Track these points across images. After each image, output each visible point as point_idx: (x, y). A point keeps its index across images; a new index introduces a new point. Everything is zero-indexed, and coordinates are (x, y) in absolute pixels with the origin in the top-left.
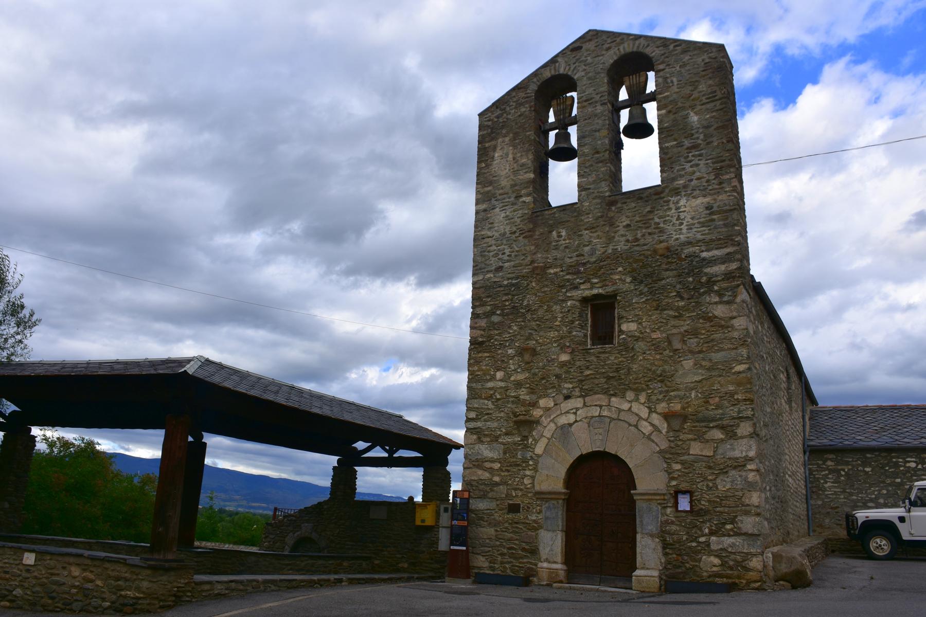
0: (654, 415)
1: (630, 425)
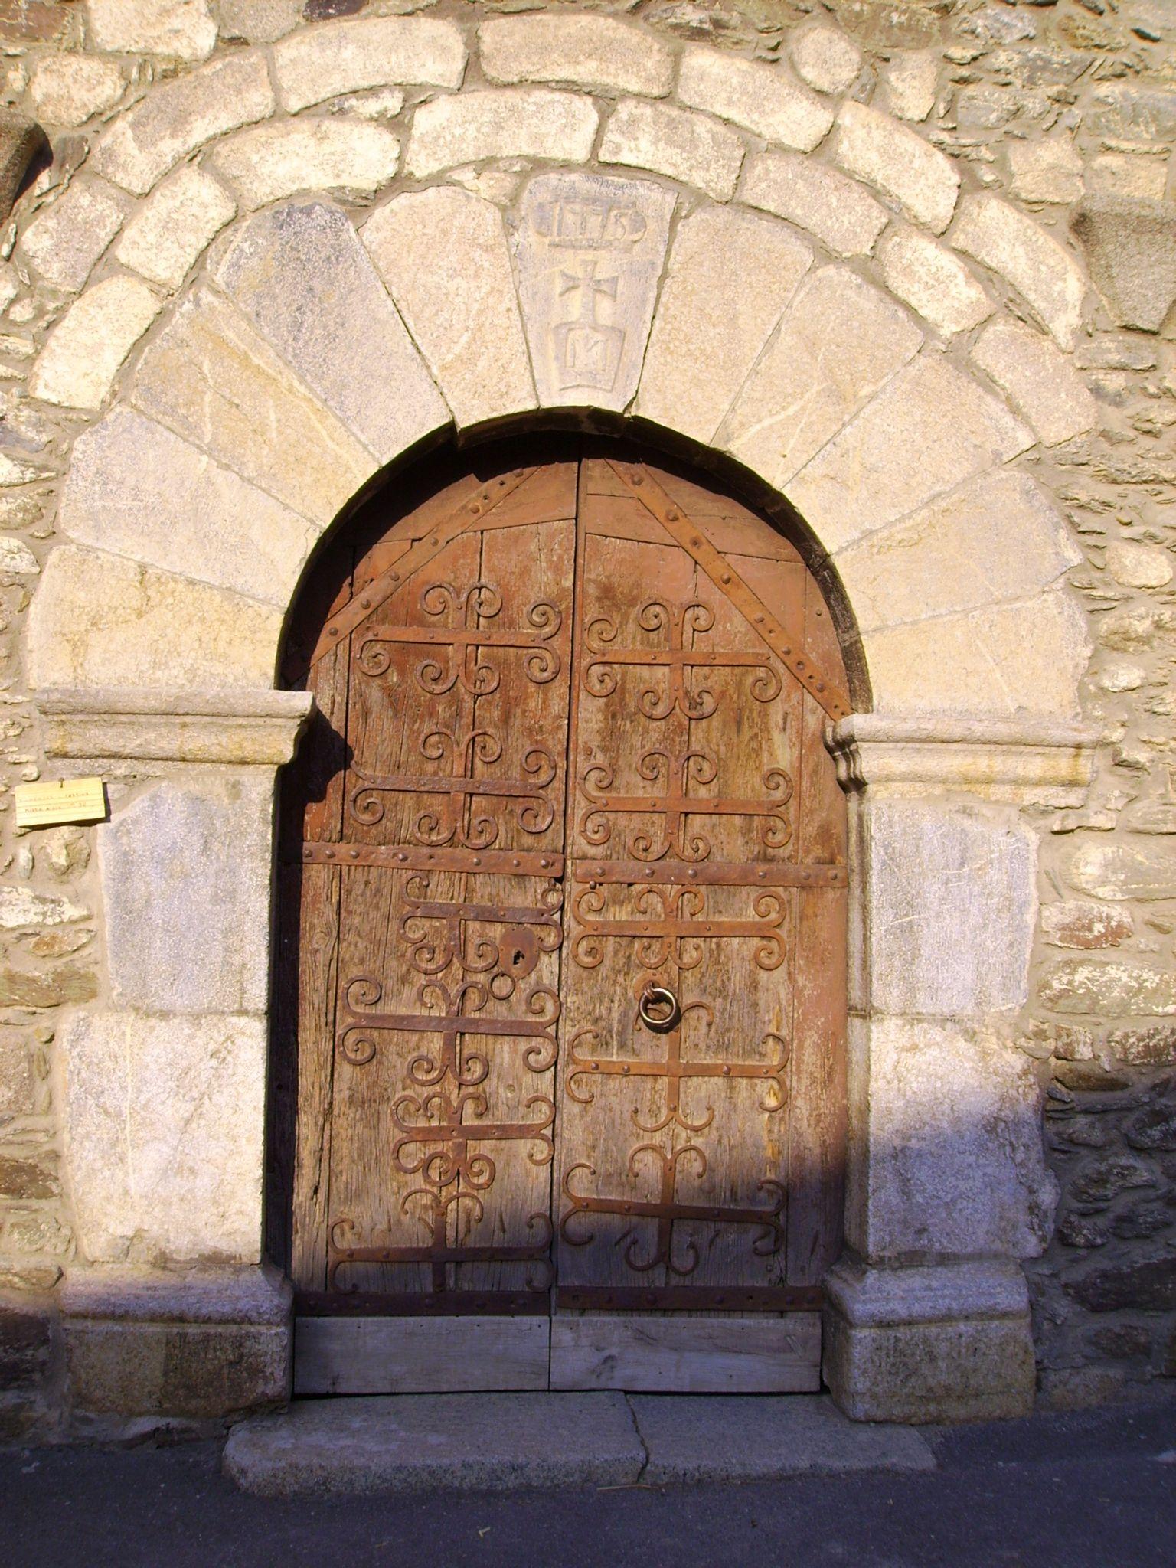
0: (993, 212)
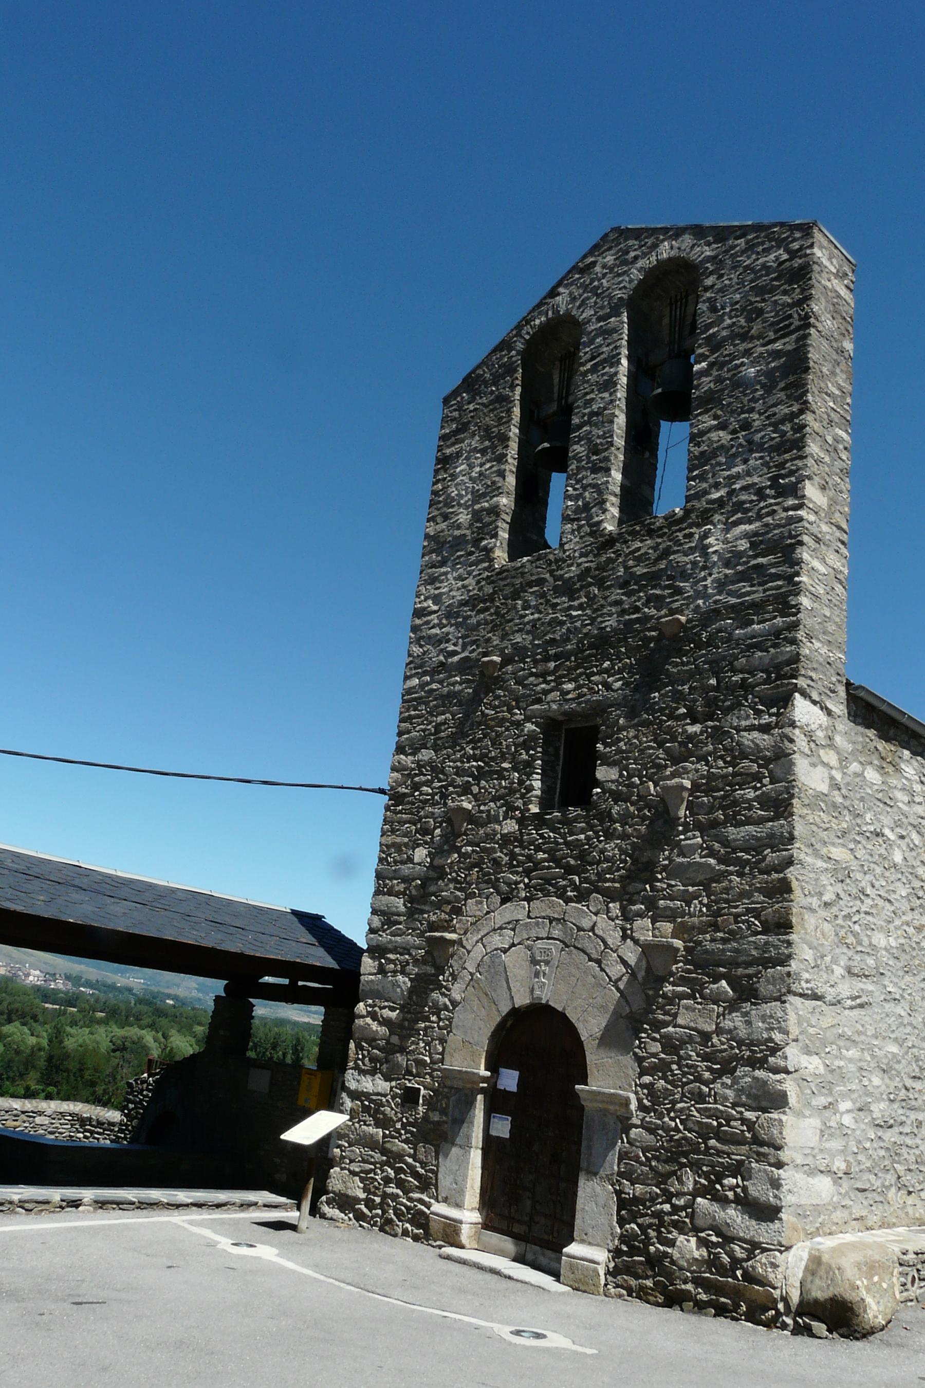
1: (590, 959)
